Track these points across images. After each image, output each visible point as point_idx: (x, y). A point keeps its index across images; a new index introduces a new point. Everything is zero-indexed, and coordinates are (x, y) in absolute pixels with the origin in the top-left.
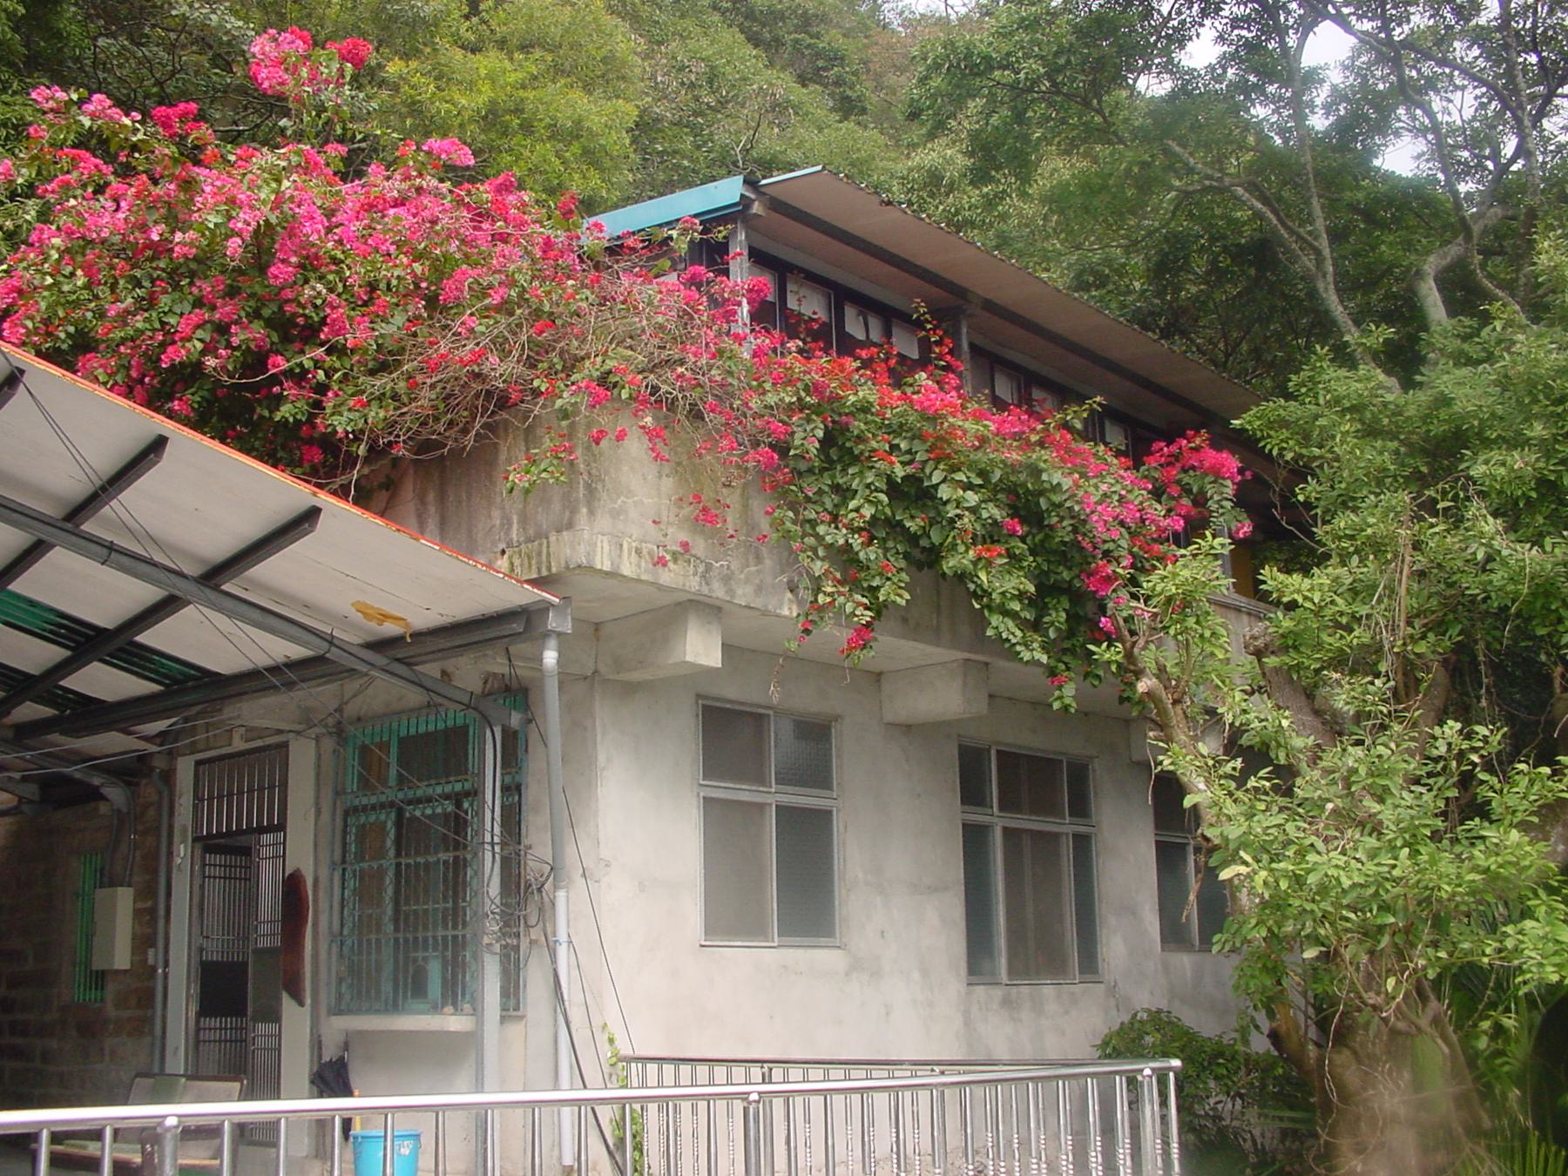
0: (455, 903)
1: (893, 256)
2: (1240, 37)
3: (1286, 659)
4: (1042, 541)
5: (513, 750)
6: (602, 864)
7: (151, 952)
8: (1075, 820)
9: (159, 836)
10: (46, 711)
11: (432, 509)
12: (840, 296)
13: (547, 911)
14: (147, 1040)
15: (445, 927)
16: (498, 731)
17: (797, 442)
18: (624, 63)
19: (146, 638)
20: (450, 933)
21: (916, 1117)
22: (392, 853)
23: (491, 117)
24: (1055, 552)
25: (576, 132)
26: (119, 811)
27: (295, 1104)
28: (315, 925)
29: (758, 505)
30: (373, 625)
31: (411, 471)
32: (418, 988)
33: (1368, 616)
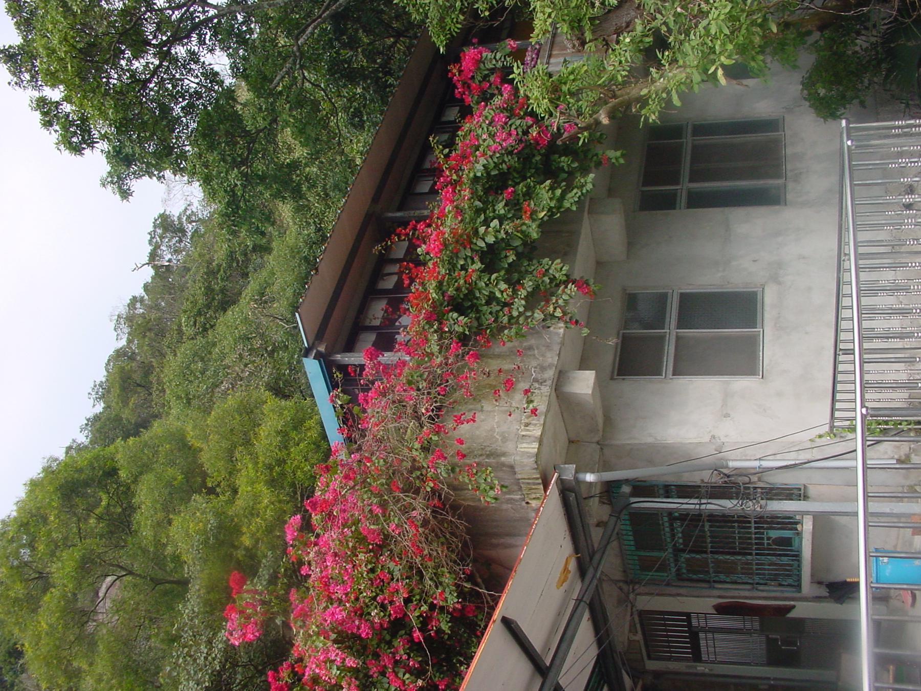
1: (347, 262)
2: (211, 39)
3: (587, 27)
4: (518, 173)
5: (643, 489)
6: (713, 441)
7: (761, 687)
8: (667, 326)
11: (502, 541)
13: (741, 472)
15: (750, 527)
16: (633, 500)
17: (461, 330)
20: (753, 525)
22: (705, 556)
23: (272, 483)
28: (746, 598)
29: (497, 349)
30: (570, 576)
32: (786, 542)
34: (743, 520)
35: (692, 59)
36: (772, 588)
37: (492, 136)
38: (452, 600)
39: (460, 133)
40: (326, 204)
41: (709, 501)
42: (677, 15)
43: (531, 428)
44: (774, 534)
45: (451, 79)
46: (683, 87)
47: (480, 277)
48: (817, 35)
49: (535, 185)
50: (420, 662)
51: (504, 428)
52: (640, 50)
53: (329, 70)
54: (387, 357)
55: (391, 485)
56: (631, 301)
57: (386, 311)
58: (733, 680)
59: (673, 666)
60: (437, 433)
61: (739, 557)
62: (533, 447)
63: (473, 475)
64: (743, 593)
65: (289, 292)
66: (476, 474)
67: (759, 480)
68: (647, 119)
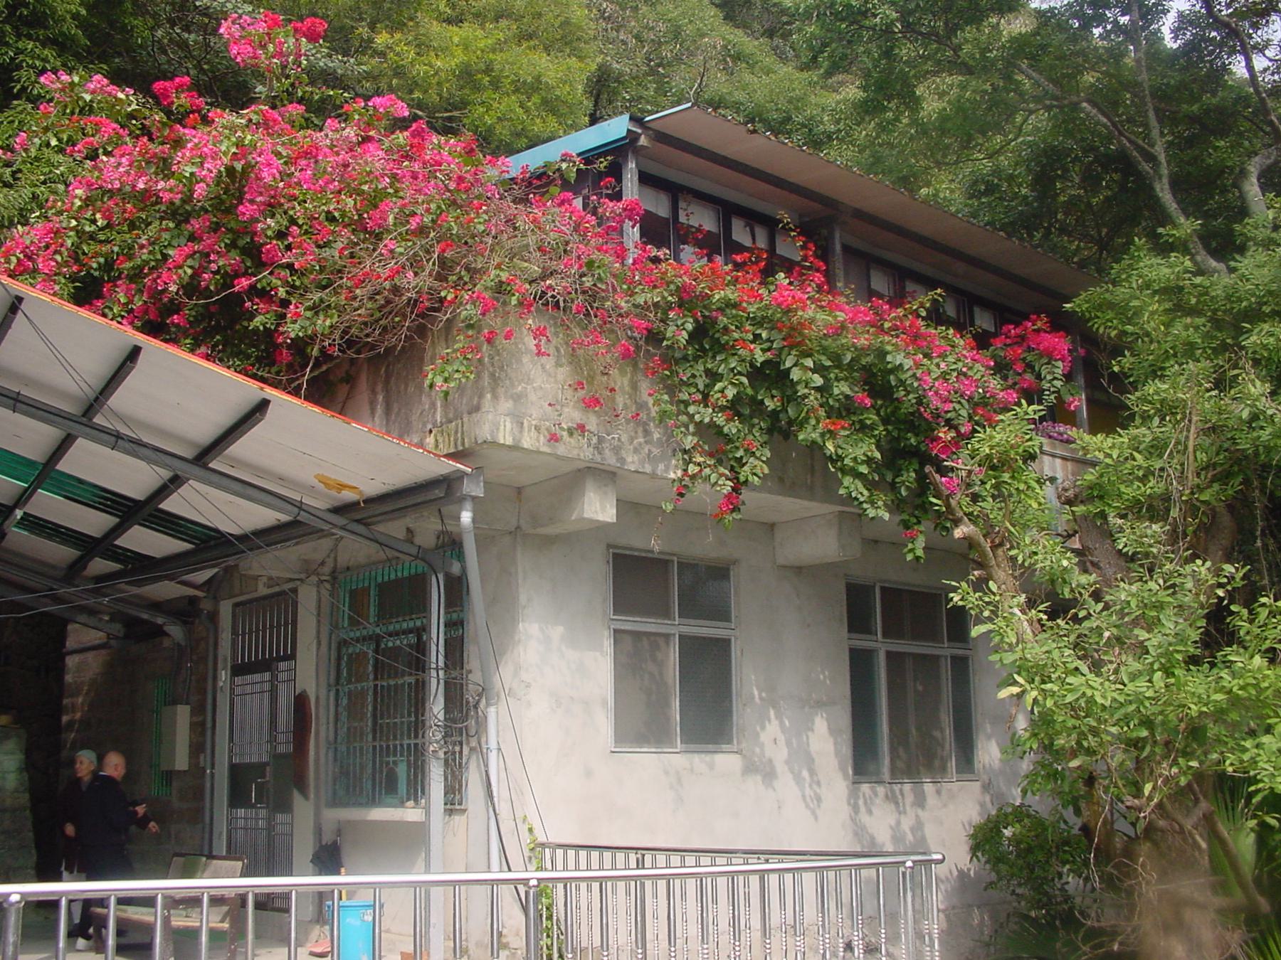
4: (893, 413)
5: (457, 590)
8: (952, 644)
10: (114, 566)
12: (727, 210)
13: (482, 724)
15: (409, 738)
16: (441, 577)
17: (669, 334)
18: (580, 28)
19: (166, 505)
20: (412, 742)
22: (371, 677)
23: (466, 75)
24: (905, 422)
25: (536, 86)
26: (179, 645)
29: (645, 386)
30: (334, 493)
31: (365, 366)
32: (390, 785)
33: (1162, 469)
34: (418, 727)
37: (944, 376)
38: (293, 330)
39: (951, 331)
40: (866, 147)
41: (442, 682)
42: (1099, 631)
43: (534, 433)
44: (402, 770)
45: (1028, 319)
46: (997, 639)
47: (743, 361)
49: (874, 436)
50: (207, 287)
51: (533, 397)
52: (1053, 581)
53: (1053, 148)
54: (632, 233)
55: (446, 240)
56: (720, 572)
58: (209, 719)
59: (226, 637)
60: (520, 303)
61: (370, 724)
62: (505, 438)
63: (464, 353)
65: (740, 96)
66: (465, 358)
67: (472, 749)
68: (955, 589)
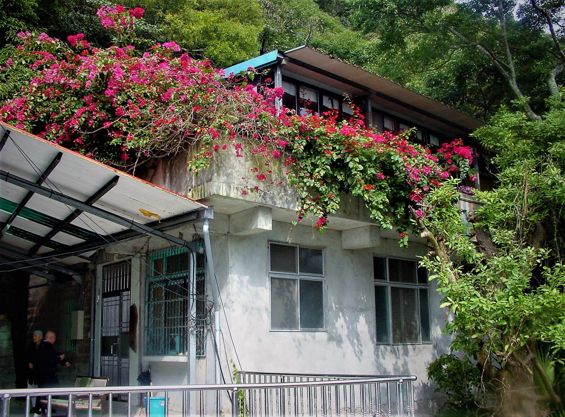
0: (184, 317)
4: (394, 182)
5: (201, 260)
7: (89, 334)
8: (420, 284)
9: (91, 293)
10: (51, 249)
13: (213, 319)
14: (88, 364)
15: (181, 325)
16: (195, 254)
17: (295, 147)
18: (256, 12)
19: (74, 222)
20: (182, 327)
21: (330, 395)
22: (164, 298)
23: (206, 33)
25: (236, 38)
27: (133, 388)
29: (284, 170)
30: (147, 217)
31: (161, 161)
32: (172, 346)
33: (513, 207)
34: (184, 320)
35: (457, 287)
36: (146, 338)
37: (417, 166)
38: (129, 145)
39: (420, 146)
40: (382, 65)
43: (235, 191)
44: (177, 339)
46: (440, 281)
47: (328, 159)
48: (475, 362)
51: (235, 175)
52: (464, 256)
53: (465, 65)
54: (279, 103)
55: (197, 106)
56: (318, 252)
57: (308, 101)
59: (100, 281)
60: (230, 133)
62: (223, 193)
63: (205, 155)
64: (142, 321)
65: (326, 42)
67: (208, 330)
68: (421, 260)
